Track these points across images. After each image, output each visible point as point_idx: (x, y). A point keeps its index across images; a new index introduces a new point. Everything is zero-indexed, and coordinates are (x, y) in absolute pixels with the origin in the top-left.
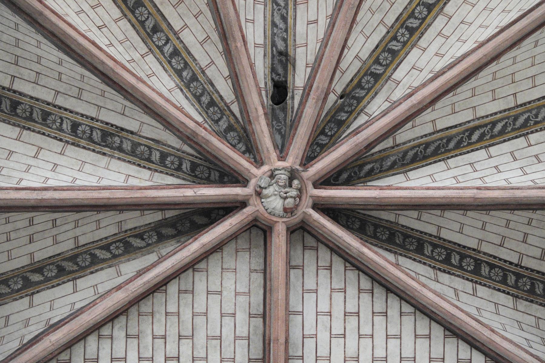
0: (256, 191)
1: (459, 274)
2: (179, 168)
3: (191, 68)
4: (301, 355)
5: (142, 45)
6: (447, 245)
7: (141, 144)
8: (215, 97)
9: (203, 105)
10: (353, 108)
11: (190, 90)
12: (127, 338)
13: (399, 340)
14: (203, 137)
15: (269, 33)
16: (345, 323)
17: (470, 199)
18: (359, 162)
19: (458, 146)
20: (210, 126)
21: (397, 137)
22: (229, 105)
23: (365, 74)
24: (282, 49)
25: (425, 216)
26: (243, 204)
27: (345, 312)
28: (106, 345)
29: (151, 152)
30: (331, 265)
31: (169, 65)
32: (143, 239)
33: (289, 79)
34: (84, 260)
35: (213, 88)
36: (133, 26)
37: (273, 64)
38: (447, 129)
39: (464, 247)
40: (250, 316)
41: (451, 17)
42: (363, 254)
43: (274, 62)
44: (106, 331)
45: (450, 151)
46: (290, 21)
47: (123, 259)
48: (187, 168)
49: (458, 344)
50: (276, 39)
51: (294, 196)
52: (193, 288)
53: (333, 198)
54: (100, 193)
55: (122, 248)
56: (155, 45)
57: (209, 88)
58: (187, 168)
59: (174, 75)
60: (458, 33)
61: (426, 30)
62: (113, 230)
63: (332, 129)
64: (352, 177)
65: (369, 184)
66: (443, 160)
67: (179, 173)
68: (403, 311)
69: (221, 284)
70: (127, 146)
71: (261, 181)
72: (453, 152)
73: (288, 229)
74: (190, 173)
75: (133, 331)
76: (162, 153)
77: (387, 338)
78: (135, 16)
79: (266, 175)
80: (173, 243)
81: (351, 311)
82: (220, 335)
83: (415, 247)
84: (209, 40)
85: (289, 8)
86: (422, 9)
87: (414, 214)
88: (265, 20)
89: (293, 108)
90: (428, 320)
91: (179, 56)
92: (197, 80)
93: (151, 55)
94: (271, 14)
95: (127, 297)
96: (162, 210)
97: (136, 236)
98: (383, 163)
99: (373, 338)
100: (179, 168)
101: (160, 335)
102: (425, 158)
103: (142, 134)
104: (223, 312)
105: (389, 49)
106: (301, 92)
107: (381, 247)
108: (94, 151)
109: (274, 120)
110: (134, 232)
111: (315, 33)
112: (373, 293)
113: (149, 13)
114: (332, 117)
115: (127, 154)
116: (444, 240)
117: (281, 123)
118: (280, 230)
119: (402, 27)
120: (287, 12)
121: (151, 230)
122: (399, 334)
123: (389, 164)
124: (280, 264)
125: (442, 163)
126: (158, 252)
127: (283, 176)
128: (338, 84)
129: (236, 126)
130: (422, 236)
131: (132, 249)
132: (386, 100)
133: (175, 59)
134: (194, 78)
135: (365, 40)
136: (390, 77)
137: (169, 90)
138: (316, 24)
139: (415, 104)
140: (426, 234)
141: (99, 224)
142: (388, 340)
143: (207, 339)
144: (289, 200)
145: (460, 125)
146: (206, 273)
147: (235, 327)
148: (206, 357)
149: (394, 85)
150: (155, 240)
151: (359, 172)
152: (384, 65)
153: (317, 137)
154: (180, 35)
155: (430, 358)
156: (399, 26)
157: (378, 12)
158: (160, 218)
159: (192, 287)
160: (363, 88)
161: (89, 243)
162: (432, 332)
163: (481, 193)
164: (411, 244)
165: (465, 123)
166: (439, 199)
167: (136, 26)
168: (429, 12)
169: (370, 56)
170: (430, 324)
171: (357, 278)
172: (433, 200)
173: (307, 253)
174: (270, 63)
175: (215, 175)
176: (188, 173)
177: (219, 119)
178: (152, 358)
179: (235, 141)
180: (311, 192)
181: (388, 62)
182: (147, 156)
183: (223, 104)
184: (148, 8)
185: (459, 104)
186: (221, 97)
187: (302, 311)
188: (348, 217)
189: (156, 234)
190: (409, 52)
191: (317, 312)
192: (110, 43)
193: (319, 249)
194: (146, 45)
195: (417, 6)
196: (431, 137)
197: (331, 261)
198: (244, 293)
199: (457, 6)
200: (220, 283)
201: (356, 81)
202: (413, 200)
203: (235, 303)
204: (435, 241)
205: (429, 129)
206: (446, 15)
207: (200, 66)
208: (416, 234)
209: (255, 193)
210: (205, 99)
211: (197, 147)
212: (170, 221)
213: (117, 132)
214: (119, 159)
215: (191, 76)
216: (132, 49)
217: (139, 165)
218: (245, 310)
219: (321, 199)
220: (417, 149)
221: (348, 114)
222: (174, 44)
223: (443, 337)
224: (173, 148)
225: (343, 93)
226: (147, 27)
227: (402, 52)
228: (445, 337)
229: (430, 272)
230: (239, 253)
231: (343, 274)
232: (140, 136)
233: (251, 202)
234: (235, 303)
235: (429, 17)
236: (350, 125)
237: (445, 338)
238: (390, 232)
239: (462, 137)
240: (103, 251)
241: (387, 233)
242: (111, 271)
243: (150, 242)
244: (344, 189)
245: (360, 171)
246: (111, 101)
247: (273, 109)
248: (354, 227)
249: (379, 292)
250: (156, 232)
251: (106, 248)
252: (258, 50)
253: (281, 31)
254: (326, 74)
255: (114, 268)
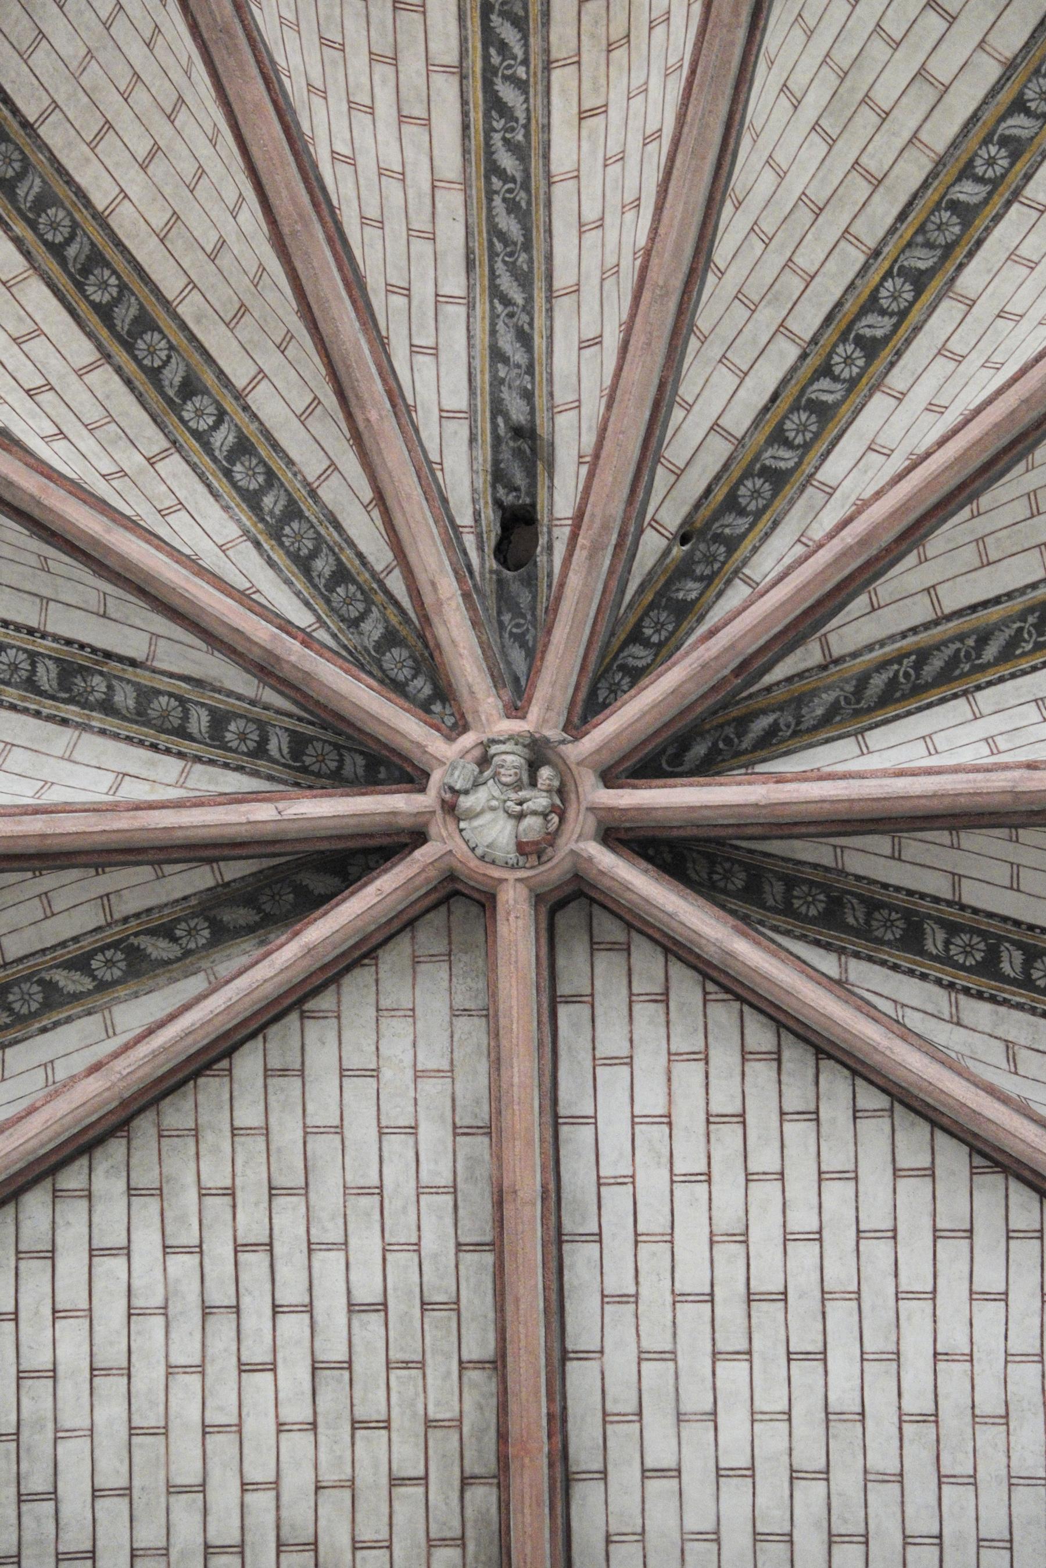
0: (443, 801)
1: (1023, 1000)
2: (260, 751)
3: (282, 485)
4: (596, 1230)
5: (151, 430)
6: (984, 924)
7: (158, 692)
8: (348, 557)
9: (317, 580)
10: (716, 566)
11: (281, 544)
12: (129, 1195)
13: (852, 1183)
14: (294, 666)
15: (483, 382)
16: (708, 1141)
17: (1002, 797)
18: (735, 712)
19: (1007, 654)
20: (334, 636)
21: (832, 638)
22: (382, 576)
23: (747, 474)
24: (522, 418)
25: (913, 847)
26: (418, 837)
27: (708, 1114)
28: (73, 1214)
29: (186, 712)
30: (667, 989)
31: (224, 480)
32: (174, 939)
33: (539, 501)
34: (27, 997)
35: (340, 535)
36: (128, 382)
37: (496, 462)
38: (974, 608)
39: (1031, 927)
40: (456, 1131)
41: (974, 302)
42: (731, 955)
43: (501, 457)
44: (72, 1178)
45: (983, 668)
46: (539, 343)
47: (122, 992)
48: (280, 750)
49: (1007, 1189)
50: (505, 395)
51: (540, 809)
52: (303, 1063)
53: (651, 810)
54: (19, 823)
55: (122, 965)
56: (189, 429)
57: (331, 535)
58: (280, 750)
59: (238, 505)
60: (986, 347)
61: (908, 342)
62: (88, 919)
63: (663, 625)
64: (720, 752)
65: (760, 768)
66: (965, 693)
67: (260, 762)
68: (861, 1104)
69: (377, 1049)
70: (125, 698)
71: (452, 775)
72: (991, 671)
73: (538, 899)
74: (291, 762)
75: (146, 1177)
76: (212, 711)
77: (820, 1180)
78: (135, 358)
79: (469, 757)
80: (246, 946)
81: (725, 1112)
82: (378, 1184)
83: (898, 933)
84: (320, 407)
85: (536, 308)
86: (898, 287)
87: (882, 843)
88: (470, 346)
89: (550, 575)
90: (926, 1127)
91: (251, 454)
92: (300, 515)
93: (176, 457)
94: (487, 328)
95: (108, 1089)
96: (209, 861)
97: (152, 932)
98: (803, 712)
99: (782, 1179)
100: (260, 751)
101: (219, 1185)
102: (917, 690)
103: (157, 664)
104: (383, 1123)
105: (810, 401)
106: (567, 530)
107: (802, 938)
108: (37, 714)
109: (504, 609)
110: (147, 922)
111: (598, 371)
112: (779, 1061)
113: (171, 347)
114: (660, 594)
115: (124, 718)
116: (976, 911)
117: (524, 617)
118: (511, 902)
119: (843, 338)
120: (532, 319)
121: (194, 915)
122: (852, 1167)
123: (819, 712)
124: (514, 992)
125: (961, 702)
126: (209, 971)
127: (510, 758)
128: (666, 504)
129: (404, 633)
130: (915, 904)
131: (144, 965)
132: (799, 540)
133: (243, 464)
134: (292, 512)
135: (737, 381)
136: (812, 476)
137: (220, 547)
138: (597, 347)
139: (851, 547)
140: (923, 896)
141: (49, 902)
142: (824, 1184)
143: (345, 1194)
144: (529, 821)
145: (1010, 595)
146: (335, 1021)
147: (417, 1161)
148: (342, 1240)
149: (821, 497)
150: (204, 941)
151: (739, 737)
152: (799, 446)
153: (621, 649)
154: (249, 400)
155: (935, 1230)
156: (835, 337)
157: (769, 303)
158: (210, 883)
159: (299, 1060)
160: (742, 512)
161: (33, 954)
162: (937, 1162)
163: (1032, 779)
164: (888, 924)
165: (1022, 591)
166: (923, 801)
167: (137, 383)
168: (918, 292)
169: (756, 423)
170: (932, 1139)
171: (738, 1023)
172: (908, 804)
173: (603, 961)
174: (489, 458)
175: (353, 765)
176: (283, 761)
177: (362, 617)
178: (200, 1246)
179: (406, 671)
180: (590, 797)
181: (809, 436)
182: (176, 723)
183: (367, 575)
184: (166, 331)
185: (999, 539)
186: (360, 555)
187: (592, 1114)
188: (712, 860)
189: (206, 924)
190: (864, 405)
191: (633, 1116)
192: (57, 431)
193: (633, 948)
194: (162, 430)
195: (884, 279)
196: (930, 632)
197: (667, 979)
198: (439, 1071)
199: (989, 271)
200: (374, 1048)
201: (720, 494)
202: (857, 807)
203: (415, 1099)
204: (951, 914)
205: (920, 612)
206: (961, 298)
207: (305, 479)
208: (897, 898)
209: (443, 807)
210: (322, 565)
211: (298, 697)
212: (238, 889)
213: (97, 662)
214: (103, 732)
215: (286, 507)
216: (124, 443)
217: (154, 747)
218: (442, 1117)
219: (617, 814)
220: (896, 667)
221: (705, 583)
222: (236, 425)
223: (968, 1173)
224: (239, 697)
225: (687, 528)
226: (166, 383)
227: (844, 408)
228: (973, 1171)
229: (939, 999)
230: (422, 968)
231: (701, 1013)
232: (154, 671)
233: (433, 831)
234: (415, 1099)
235: (918, 306)
236: (707, 612)
237: (972, 1174)
238: (828, 896)
239: (1020, 630)
240: (73, 973)
241: (822, 897)
242: (91, 1025)
243: (192, 945)
244: (683, 785)
245: (741, 735)
246: (70, 584)
247: (501, 582)
248: (730, 886)
249: (795, 1055)
250: (206, 919)
251: (81, 964)
252: (450, 426)
253: (516, 371)
254: (610, 479)
255: (97, 1018)
